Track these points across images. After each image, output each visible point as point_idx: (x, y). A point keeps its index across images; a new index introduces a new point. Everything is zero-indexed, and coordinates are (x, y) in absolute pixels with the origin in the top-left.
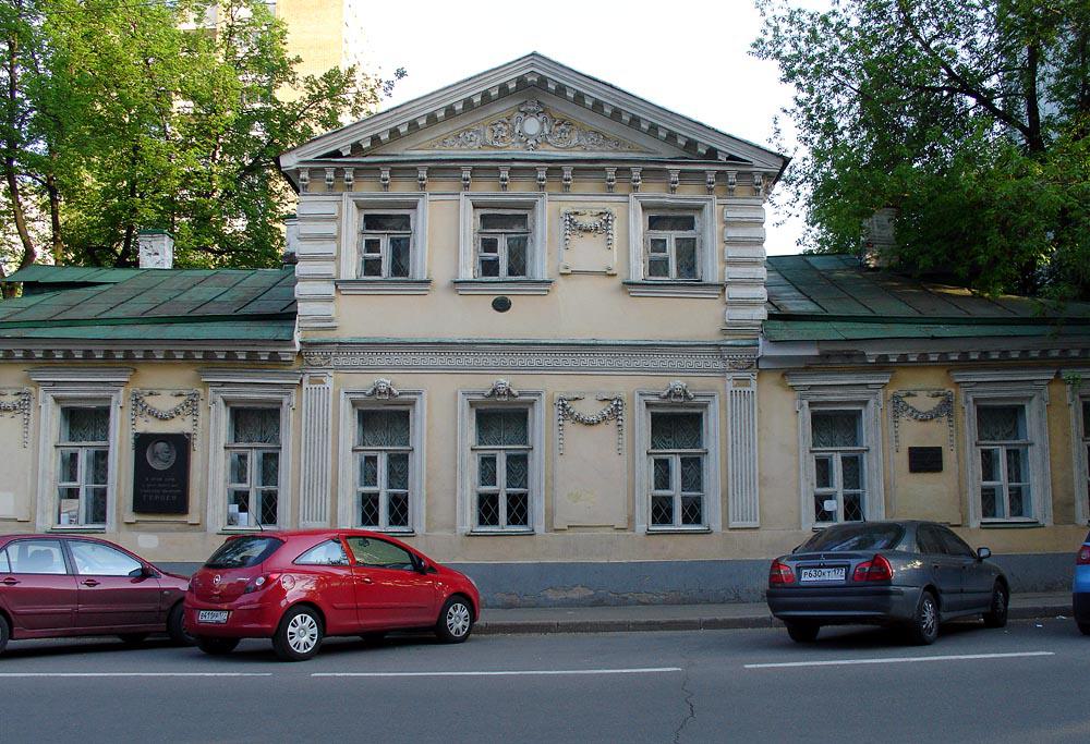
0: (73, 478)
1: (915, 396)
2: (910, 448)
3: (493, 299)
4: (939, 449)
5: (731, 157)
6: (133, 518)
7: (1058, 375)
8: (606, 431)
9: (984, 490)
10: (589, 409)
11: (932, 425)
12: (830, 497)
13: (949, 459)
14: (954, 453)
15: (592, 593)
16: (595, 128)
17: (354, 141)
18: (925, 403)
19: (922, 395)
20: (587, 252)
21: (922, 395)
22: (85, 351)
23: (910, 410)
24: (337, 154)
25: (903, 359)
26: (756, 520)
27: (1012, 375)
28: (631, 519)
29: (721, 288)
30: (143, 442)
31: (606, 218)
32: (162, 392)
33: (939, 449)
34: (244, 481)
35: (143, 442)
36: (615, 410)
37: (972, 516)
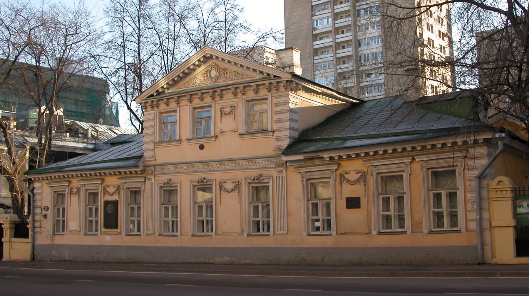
0: (388, 210)
1: (110, 187)
2: (346, 198)
3: (199, 145)
4: (359, 198)
5: (275, 76)
6: (104, 230)
7: (413, 159)
8: (235, 194)
9: (269, 218)
10: (229, 186)
11: (357, 186)
12: (318, 220)
13: (363, 202)
14: (366, 200)
15: (230, 259)
16: (235, 71)
17: (156, 90)
18: (353, 176)
19: (352, 173)
20: (228, 123)
21: (352, 173)
22: (365, 153)
23: (356, 182)
24: (152, 96)
25: (340, 157)
26: (285, 231)
27: (94, 182)
28: (242, 230)
29: (179, 142)
30: (106, 203)
31: (233, 109)
32: (111, 186)
33: (359, 198)
34: (317, 215)
35: (106, 203)
36: (237, 186)
37: (373, 229)
